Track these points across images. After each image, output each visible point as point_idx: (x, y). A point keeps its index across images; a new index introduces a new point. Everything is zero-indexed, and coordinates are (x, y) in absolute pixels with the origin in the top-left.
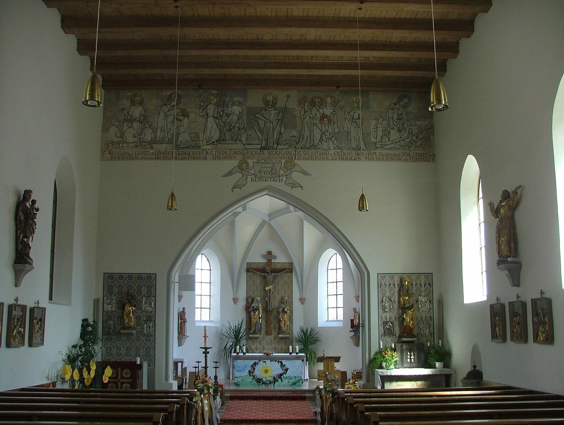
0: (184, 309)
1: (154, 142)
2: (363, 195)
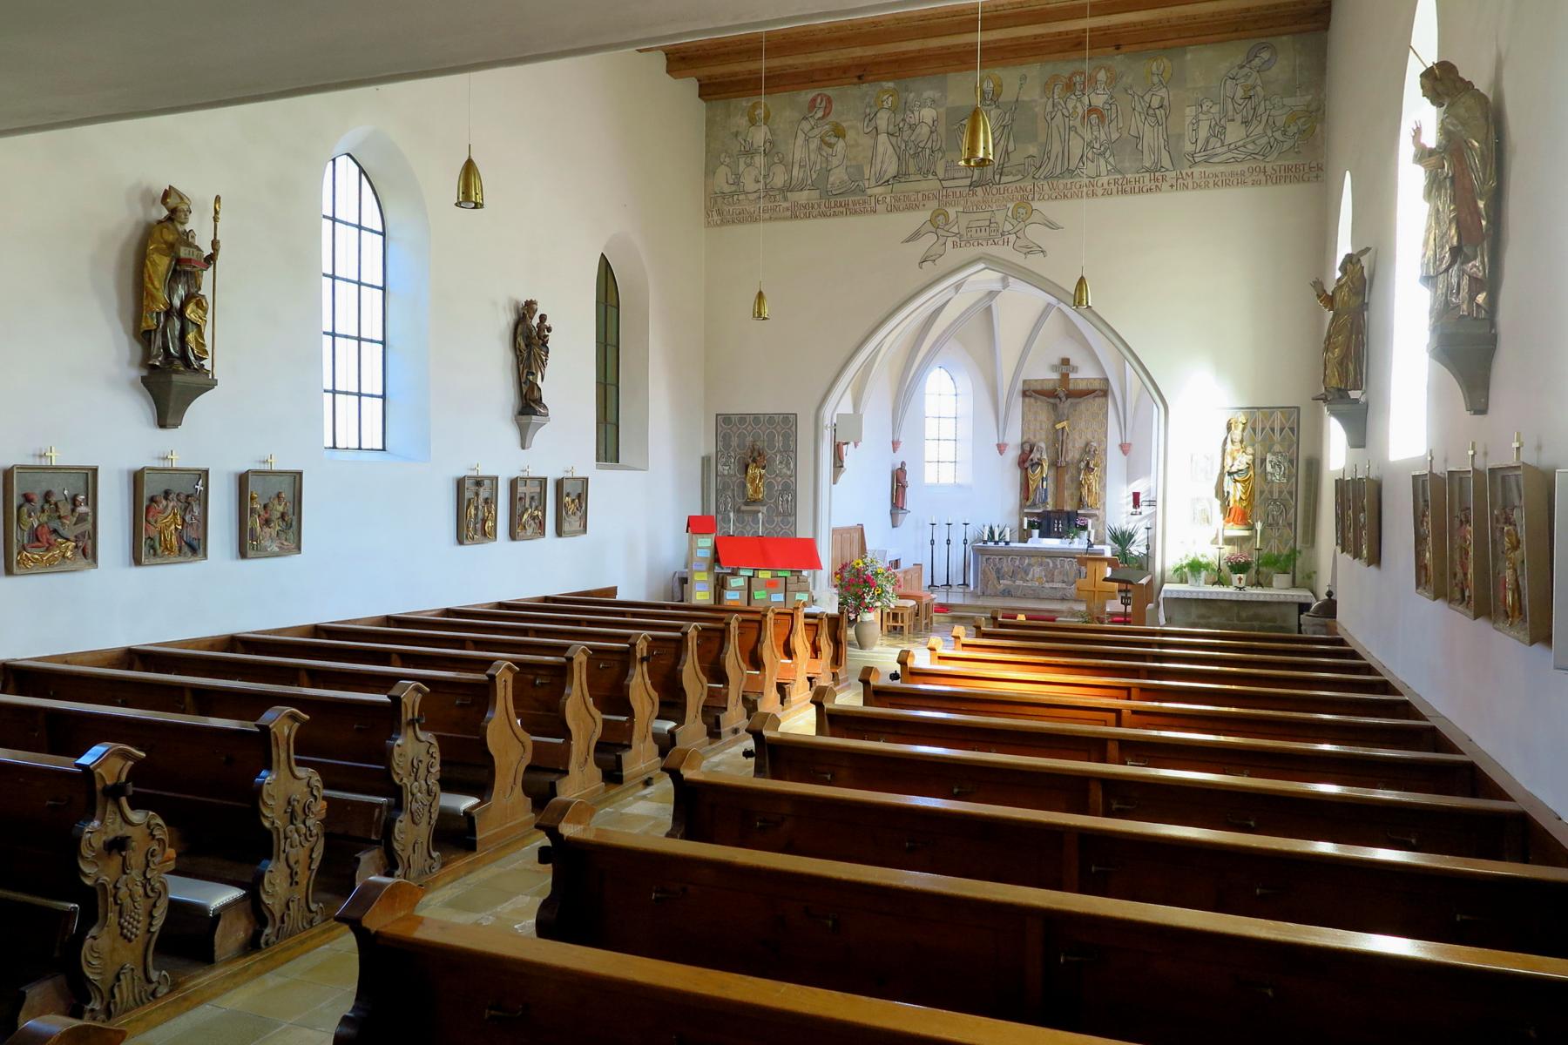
0: (903, 464)
1: (788, 188)
2: (1082, 279)
